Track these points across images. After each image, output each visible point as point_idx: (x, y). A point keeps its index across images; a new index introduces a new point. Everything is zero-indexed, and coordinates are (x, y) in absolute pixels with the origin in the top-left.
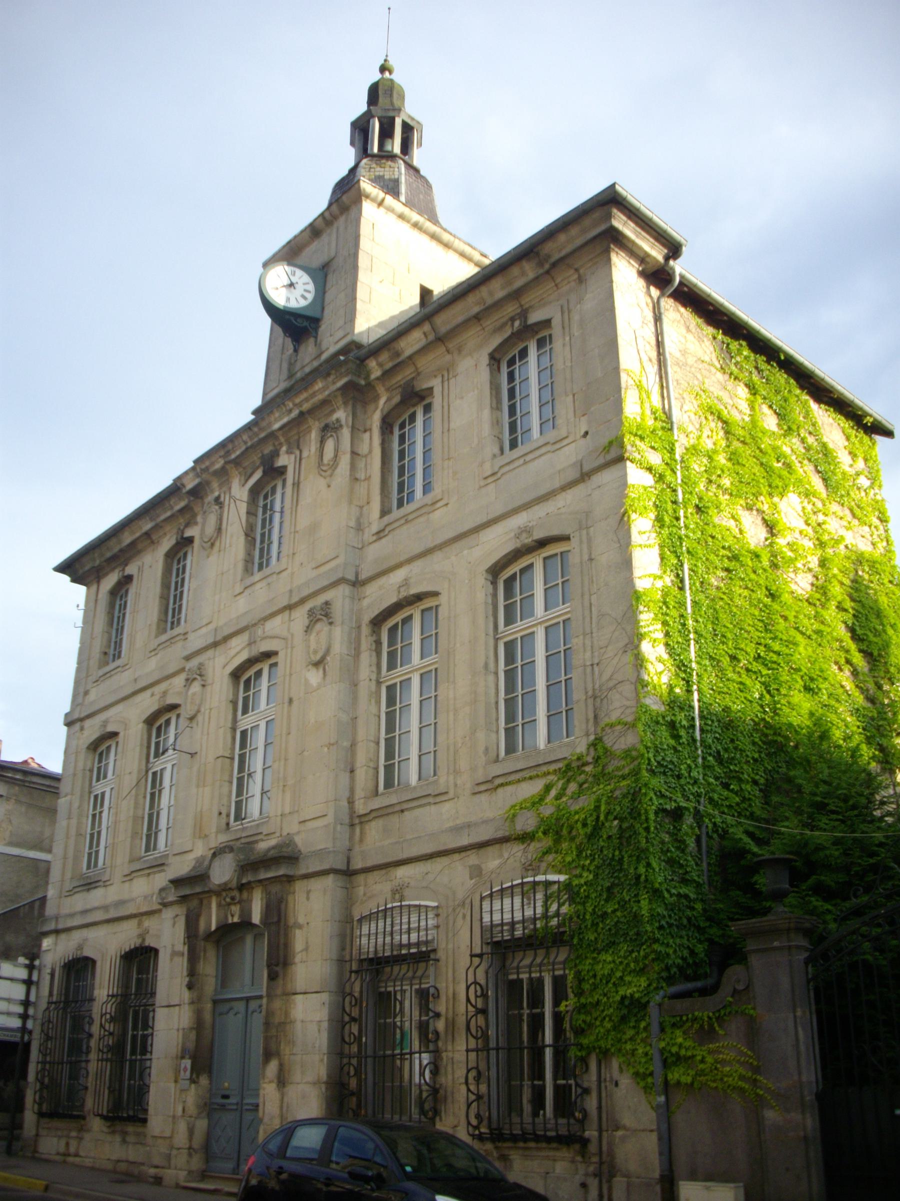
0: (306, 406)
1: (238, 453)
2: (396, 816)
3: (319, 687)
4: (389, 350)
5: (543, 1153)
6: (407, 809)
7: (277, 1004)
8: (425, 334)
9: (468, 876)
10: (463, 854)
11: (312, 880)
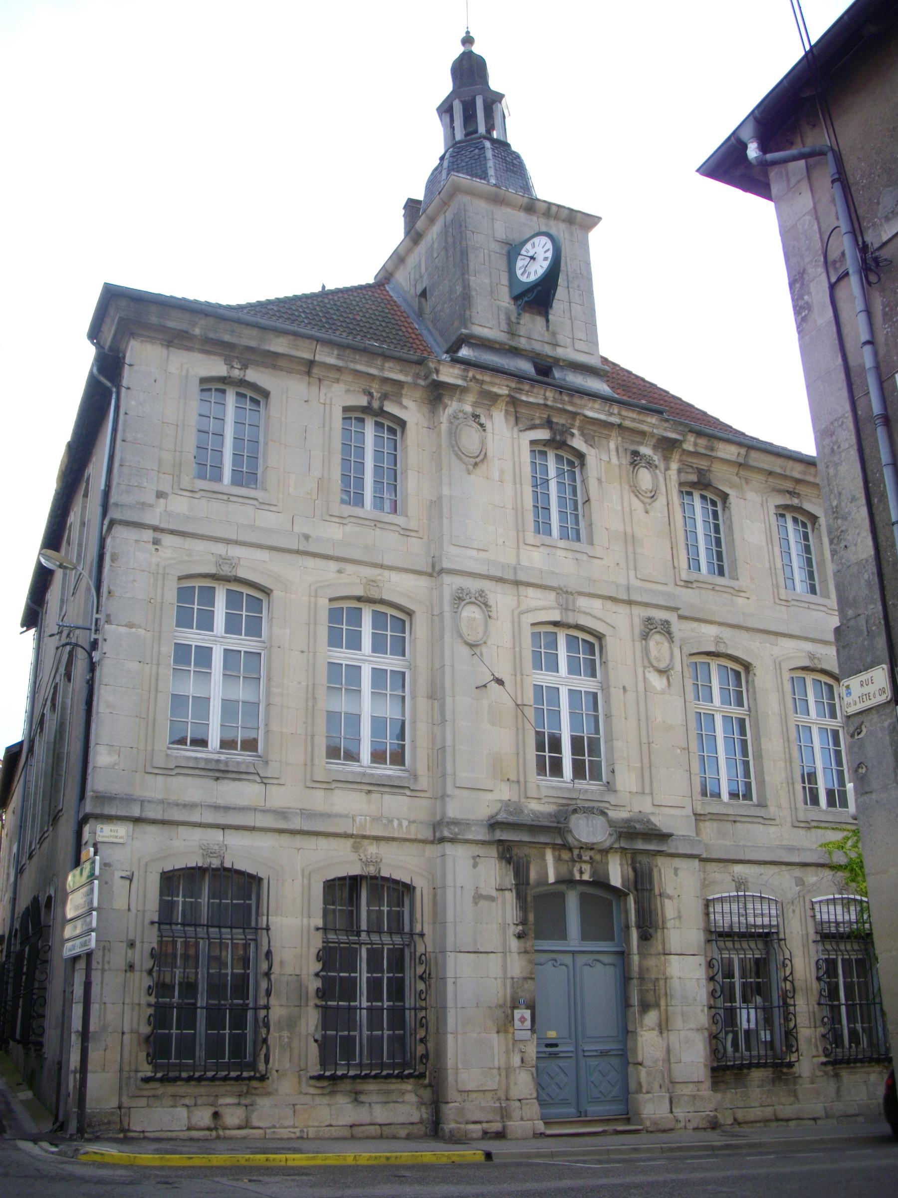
0: (627, 423)
1: (531, 400)
2: (729, 823)
3: (663, 692)
4: (709, 441)
5: (863, 1070)
6: (741, 822)
7: (651, 962)
8: (739, 453)
9: (794, 883)
10: (790, 867)
11: (677, 859)
